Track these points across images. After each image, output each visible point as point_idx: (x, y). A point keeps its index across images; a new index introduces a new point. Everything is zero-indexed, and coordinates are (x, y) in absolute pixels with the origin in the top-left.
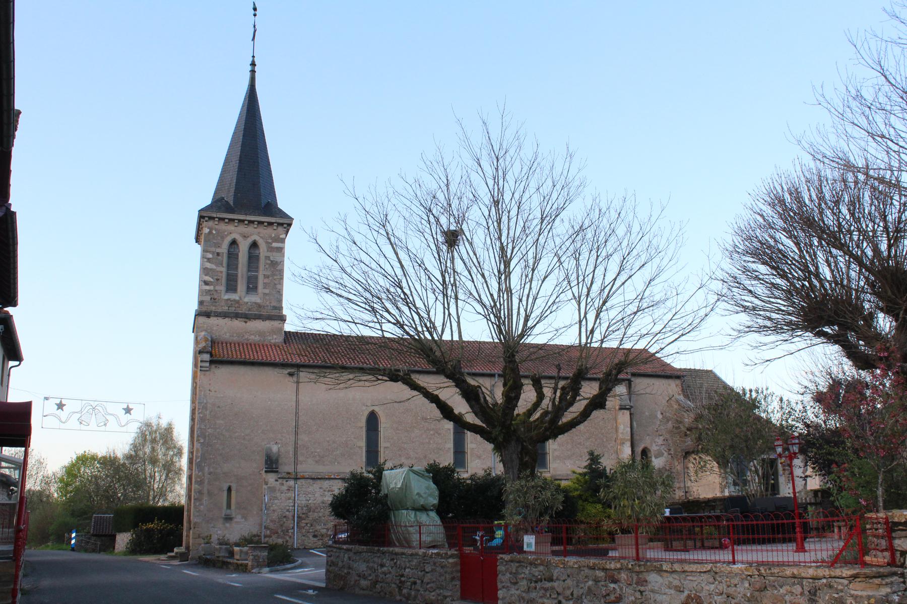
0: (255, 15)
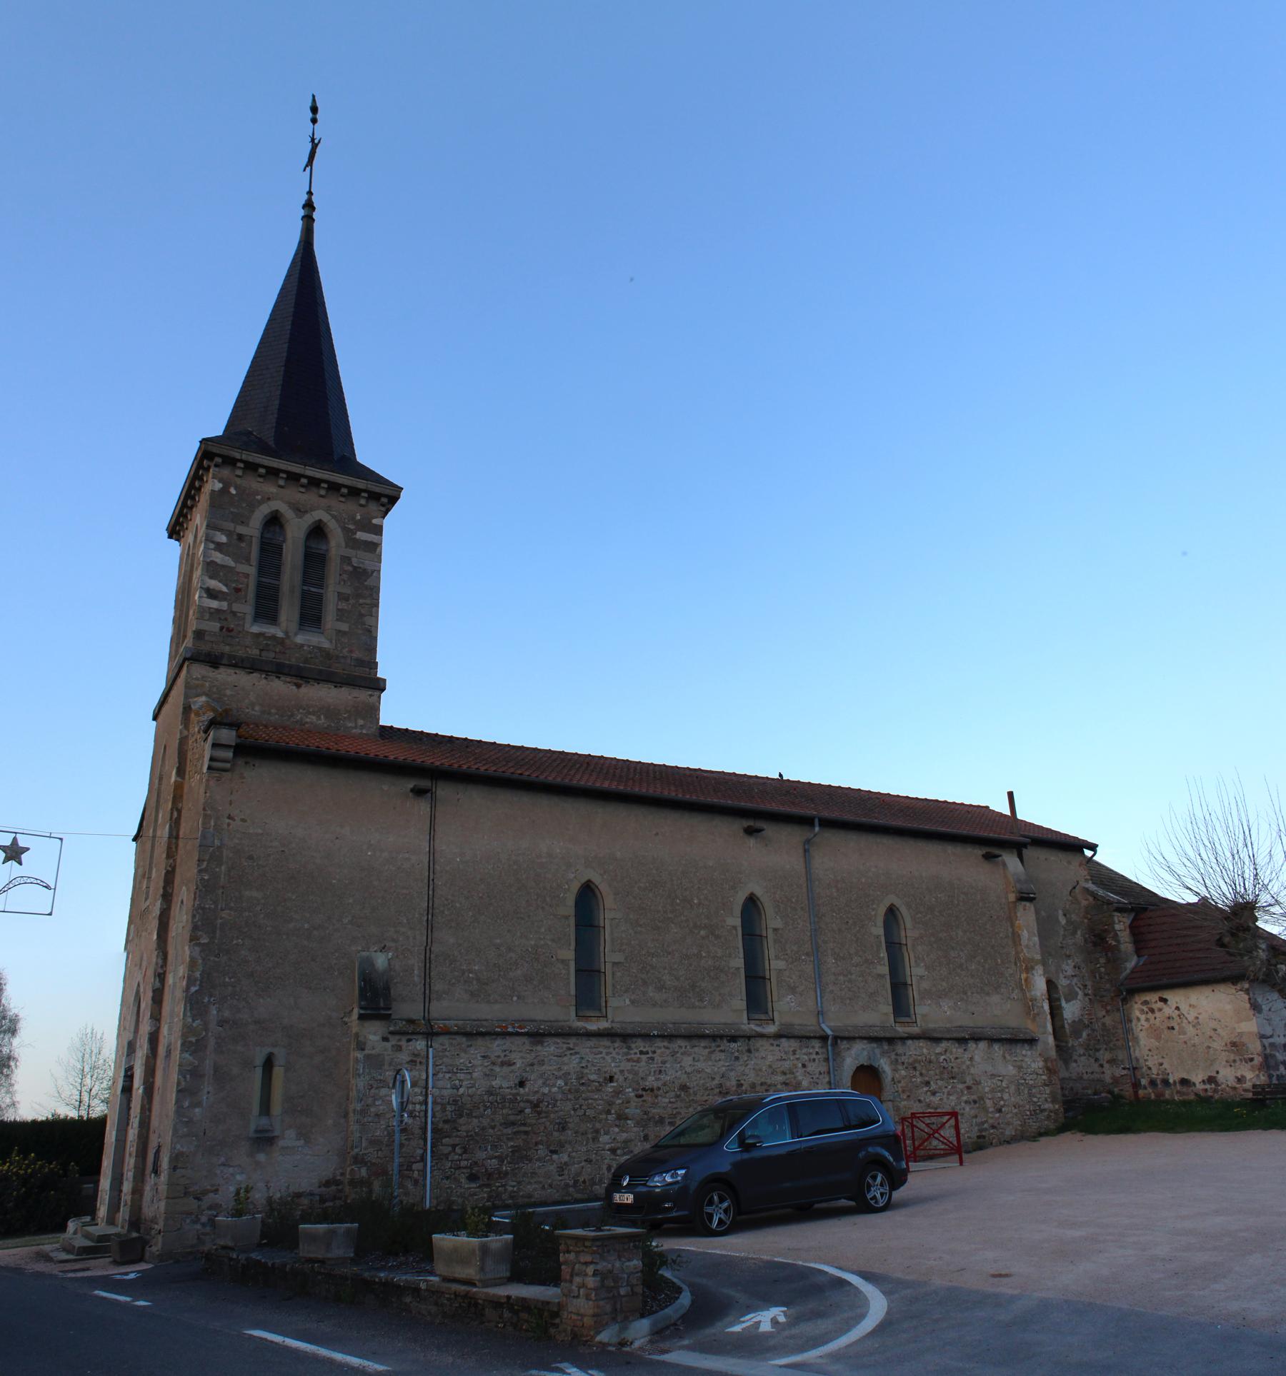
0: (314, 121)
